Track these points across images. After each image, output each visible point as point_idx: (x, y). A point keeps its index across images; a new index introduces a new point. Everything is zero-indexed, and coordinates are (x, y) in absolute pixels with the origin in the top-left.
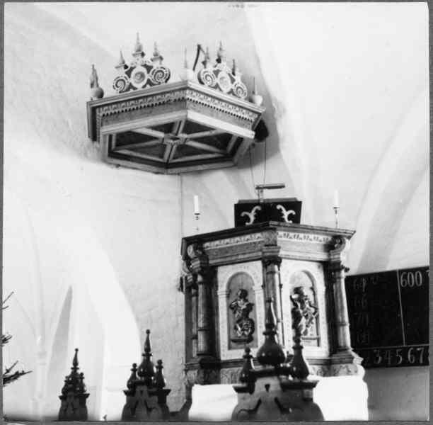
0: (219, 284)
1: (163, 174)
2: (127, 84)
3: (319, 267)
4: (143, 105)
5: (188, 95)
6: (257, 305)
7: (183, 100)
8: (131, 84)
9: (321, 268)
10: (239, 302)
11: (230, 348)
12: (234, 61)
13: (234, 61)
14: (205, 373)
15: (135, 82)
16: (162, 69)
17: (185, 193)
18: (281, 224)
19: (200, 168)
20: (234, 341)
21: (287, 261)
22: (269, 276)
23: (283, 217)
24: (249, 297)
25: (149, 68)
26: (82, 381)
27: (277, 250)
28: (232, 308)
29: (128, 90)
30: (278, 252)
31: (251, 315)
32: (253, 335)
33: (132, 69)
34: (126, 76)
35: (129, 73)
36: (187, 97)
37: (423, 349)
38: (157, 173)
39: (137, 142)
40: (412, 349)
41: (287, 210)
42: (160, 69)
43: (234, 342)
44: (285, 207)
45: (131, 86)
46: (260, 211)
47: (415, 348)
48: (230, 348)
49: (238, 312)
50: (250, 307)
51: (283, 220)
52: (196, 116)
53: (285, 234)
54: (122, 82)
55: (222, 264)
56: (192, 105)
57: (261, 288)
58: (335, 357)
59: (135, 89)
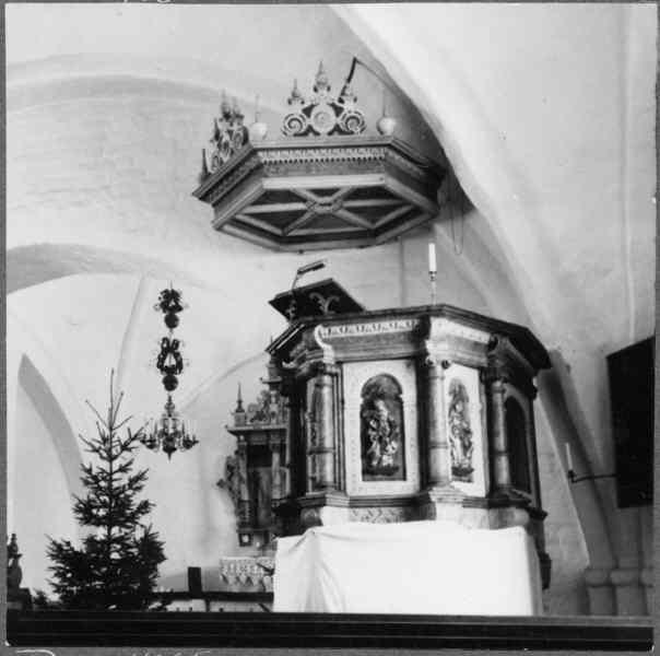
1: (368, 246)
2: (305, 127)
3: (408, 366)
5: (263, 157)
7: (260, 167)
9: (412, 367)
12: (295, 82)
13: (295, 82)
14: (284, 522)
15: (329, 116)
17: (407, 264)
18: (319, 318)
19: (302, 246)
21: (350, 365)
22: (318, 390)
23: (321, 308)
27: (320, 354)
29: (305, 134)
30: (323, 356)
33: (312, 107)
35: (308, 111)
36: (263, 161)
38: (362, 247)
39: (295, 220)
41: (326, 298)
44: (322, 294)
45: (310, 129)
46: (337, 303)
51: (321, 313)
52: (274, 183)
56: (272, 169)
58: (512, 498)
59: (317, 134)
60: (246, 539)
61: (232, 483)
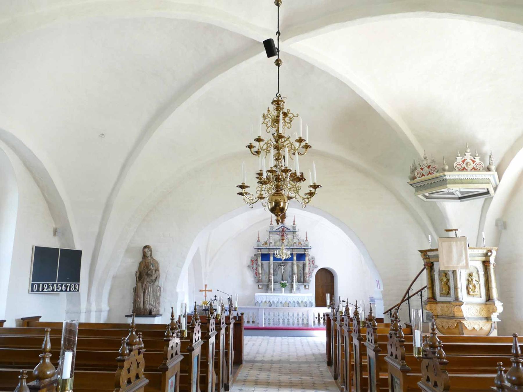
0: (435, 269)
4: (422, 185)
6: (451, 280)
8: (464, 167)
10: (443, 278)
11: (441, 296)
16: (476, 164)
20: (442, 294)
24: (447, 276)
25: (429, 167)
26: (349, 311)
28: (441, 280)
31: (448, 283)
32: (450, 292)
34: (462, 163)
37: (70, 284)
40: (65, 284)
42: (479, 163)
43: (442, 295)
47: (66, 284)
48: (441, 296)
49: (442, 282)
50: (448, 280)
53: (477, 251)
54: (458, 165)
55: (435, 261)
57: (452, 273)
60: (260, 287)
61: (253, 266)
